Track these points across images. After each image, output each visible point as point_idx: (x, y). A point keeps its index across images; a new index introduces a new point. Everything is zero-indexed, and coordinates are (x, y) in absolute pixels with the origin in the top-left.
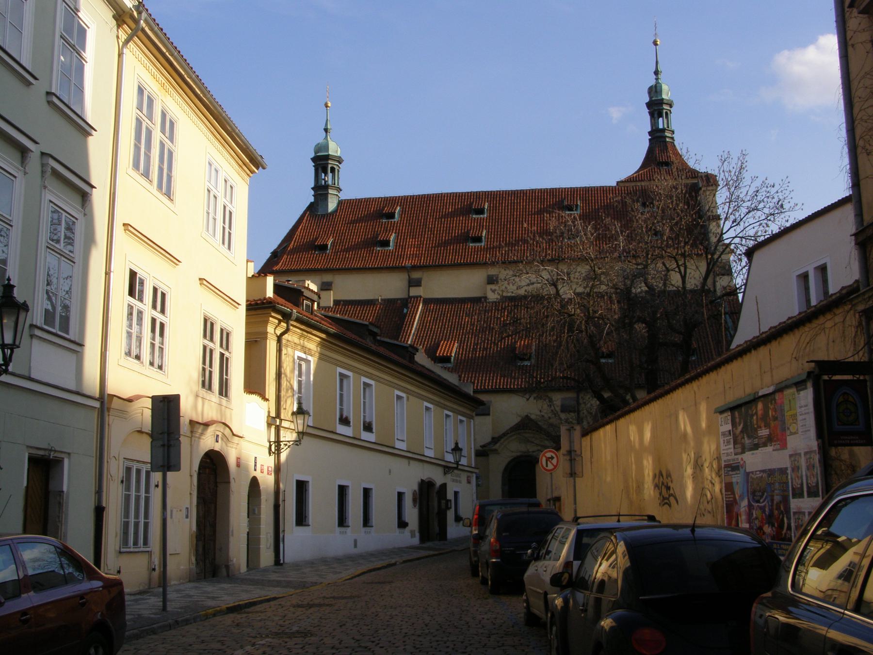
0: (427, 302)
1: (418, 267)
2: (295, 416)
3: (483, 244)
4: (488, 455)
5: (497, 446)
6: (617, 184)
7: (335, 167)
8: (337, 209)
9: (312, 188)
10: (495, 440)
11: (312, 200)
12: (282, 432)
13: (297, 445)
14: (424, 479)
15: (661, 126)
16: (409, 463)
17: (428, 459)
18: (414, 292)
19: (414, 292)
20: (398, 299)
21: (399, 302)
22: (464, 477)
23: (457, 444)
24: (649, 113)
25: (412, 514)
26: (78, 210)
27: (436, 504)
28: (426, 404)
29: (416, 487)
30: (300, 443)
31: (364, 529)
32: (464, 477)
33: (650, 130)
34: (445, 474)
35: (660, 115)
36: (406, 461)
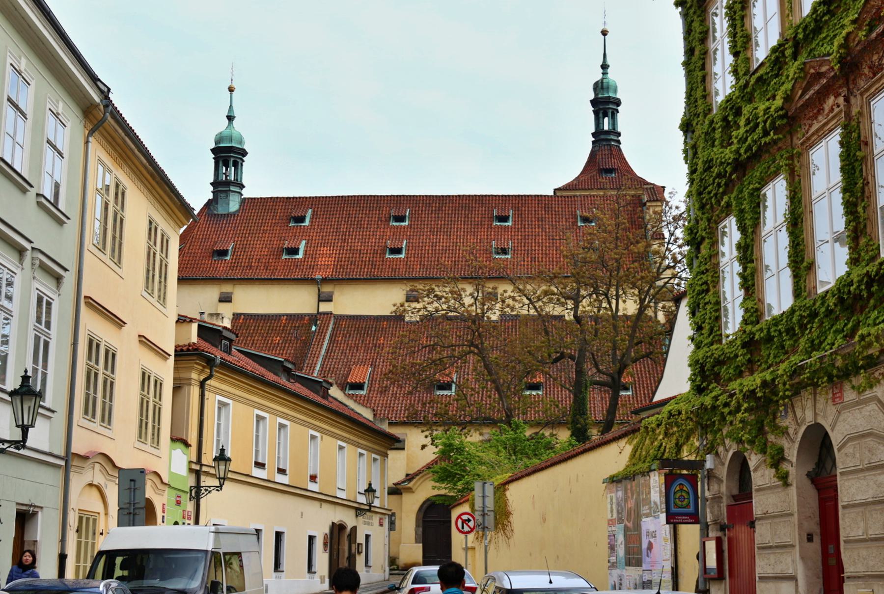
0: (340, 318)
1: (329, 280)
2: (216, 462)
3: (403, 256)
4: (401, 494)
5: (410, 485)
6: (554, 192)
7: (238, 160)
8: (240, 209)
9: (211, 184)
10: (410, 478)
11: (211, 196)
12: (203, 478)
13: (217, 490)
14: (335, 521)
15: (606, 128)
16: (321, 505)
17: (340, 501)
18: (325, 307)
19: (325, 307)
20: (305, 315)
21: (307, 318)
22: (376, 519)
23: (370, 484)
24: (594, 111)
25: (322, 560)
26: (53, 291)
27: (346, 548)
28: (340, 443)
29: (327, 531)
30: (221, 489)
31: (274, 574)
32: (376, 519)
33: (593, 131)
34: (357, 516)
35: (605, 115)
36: (317, 504)
